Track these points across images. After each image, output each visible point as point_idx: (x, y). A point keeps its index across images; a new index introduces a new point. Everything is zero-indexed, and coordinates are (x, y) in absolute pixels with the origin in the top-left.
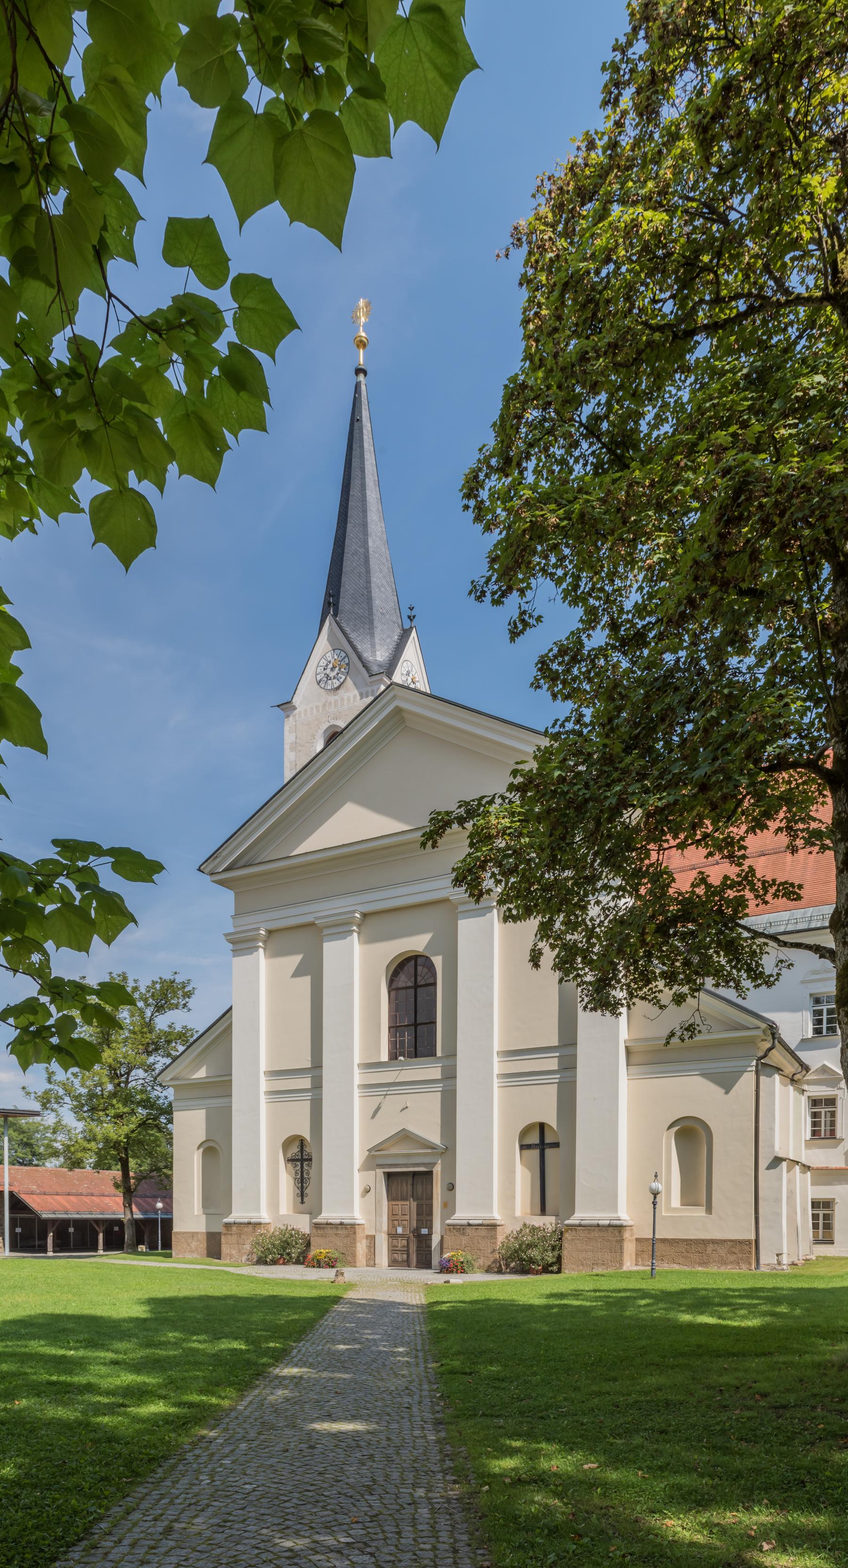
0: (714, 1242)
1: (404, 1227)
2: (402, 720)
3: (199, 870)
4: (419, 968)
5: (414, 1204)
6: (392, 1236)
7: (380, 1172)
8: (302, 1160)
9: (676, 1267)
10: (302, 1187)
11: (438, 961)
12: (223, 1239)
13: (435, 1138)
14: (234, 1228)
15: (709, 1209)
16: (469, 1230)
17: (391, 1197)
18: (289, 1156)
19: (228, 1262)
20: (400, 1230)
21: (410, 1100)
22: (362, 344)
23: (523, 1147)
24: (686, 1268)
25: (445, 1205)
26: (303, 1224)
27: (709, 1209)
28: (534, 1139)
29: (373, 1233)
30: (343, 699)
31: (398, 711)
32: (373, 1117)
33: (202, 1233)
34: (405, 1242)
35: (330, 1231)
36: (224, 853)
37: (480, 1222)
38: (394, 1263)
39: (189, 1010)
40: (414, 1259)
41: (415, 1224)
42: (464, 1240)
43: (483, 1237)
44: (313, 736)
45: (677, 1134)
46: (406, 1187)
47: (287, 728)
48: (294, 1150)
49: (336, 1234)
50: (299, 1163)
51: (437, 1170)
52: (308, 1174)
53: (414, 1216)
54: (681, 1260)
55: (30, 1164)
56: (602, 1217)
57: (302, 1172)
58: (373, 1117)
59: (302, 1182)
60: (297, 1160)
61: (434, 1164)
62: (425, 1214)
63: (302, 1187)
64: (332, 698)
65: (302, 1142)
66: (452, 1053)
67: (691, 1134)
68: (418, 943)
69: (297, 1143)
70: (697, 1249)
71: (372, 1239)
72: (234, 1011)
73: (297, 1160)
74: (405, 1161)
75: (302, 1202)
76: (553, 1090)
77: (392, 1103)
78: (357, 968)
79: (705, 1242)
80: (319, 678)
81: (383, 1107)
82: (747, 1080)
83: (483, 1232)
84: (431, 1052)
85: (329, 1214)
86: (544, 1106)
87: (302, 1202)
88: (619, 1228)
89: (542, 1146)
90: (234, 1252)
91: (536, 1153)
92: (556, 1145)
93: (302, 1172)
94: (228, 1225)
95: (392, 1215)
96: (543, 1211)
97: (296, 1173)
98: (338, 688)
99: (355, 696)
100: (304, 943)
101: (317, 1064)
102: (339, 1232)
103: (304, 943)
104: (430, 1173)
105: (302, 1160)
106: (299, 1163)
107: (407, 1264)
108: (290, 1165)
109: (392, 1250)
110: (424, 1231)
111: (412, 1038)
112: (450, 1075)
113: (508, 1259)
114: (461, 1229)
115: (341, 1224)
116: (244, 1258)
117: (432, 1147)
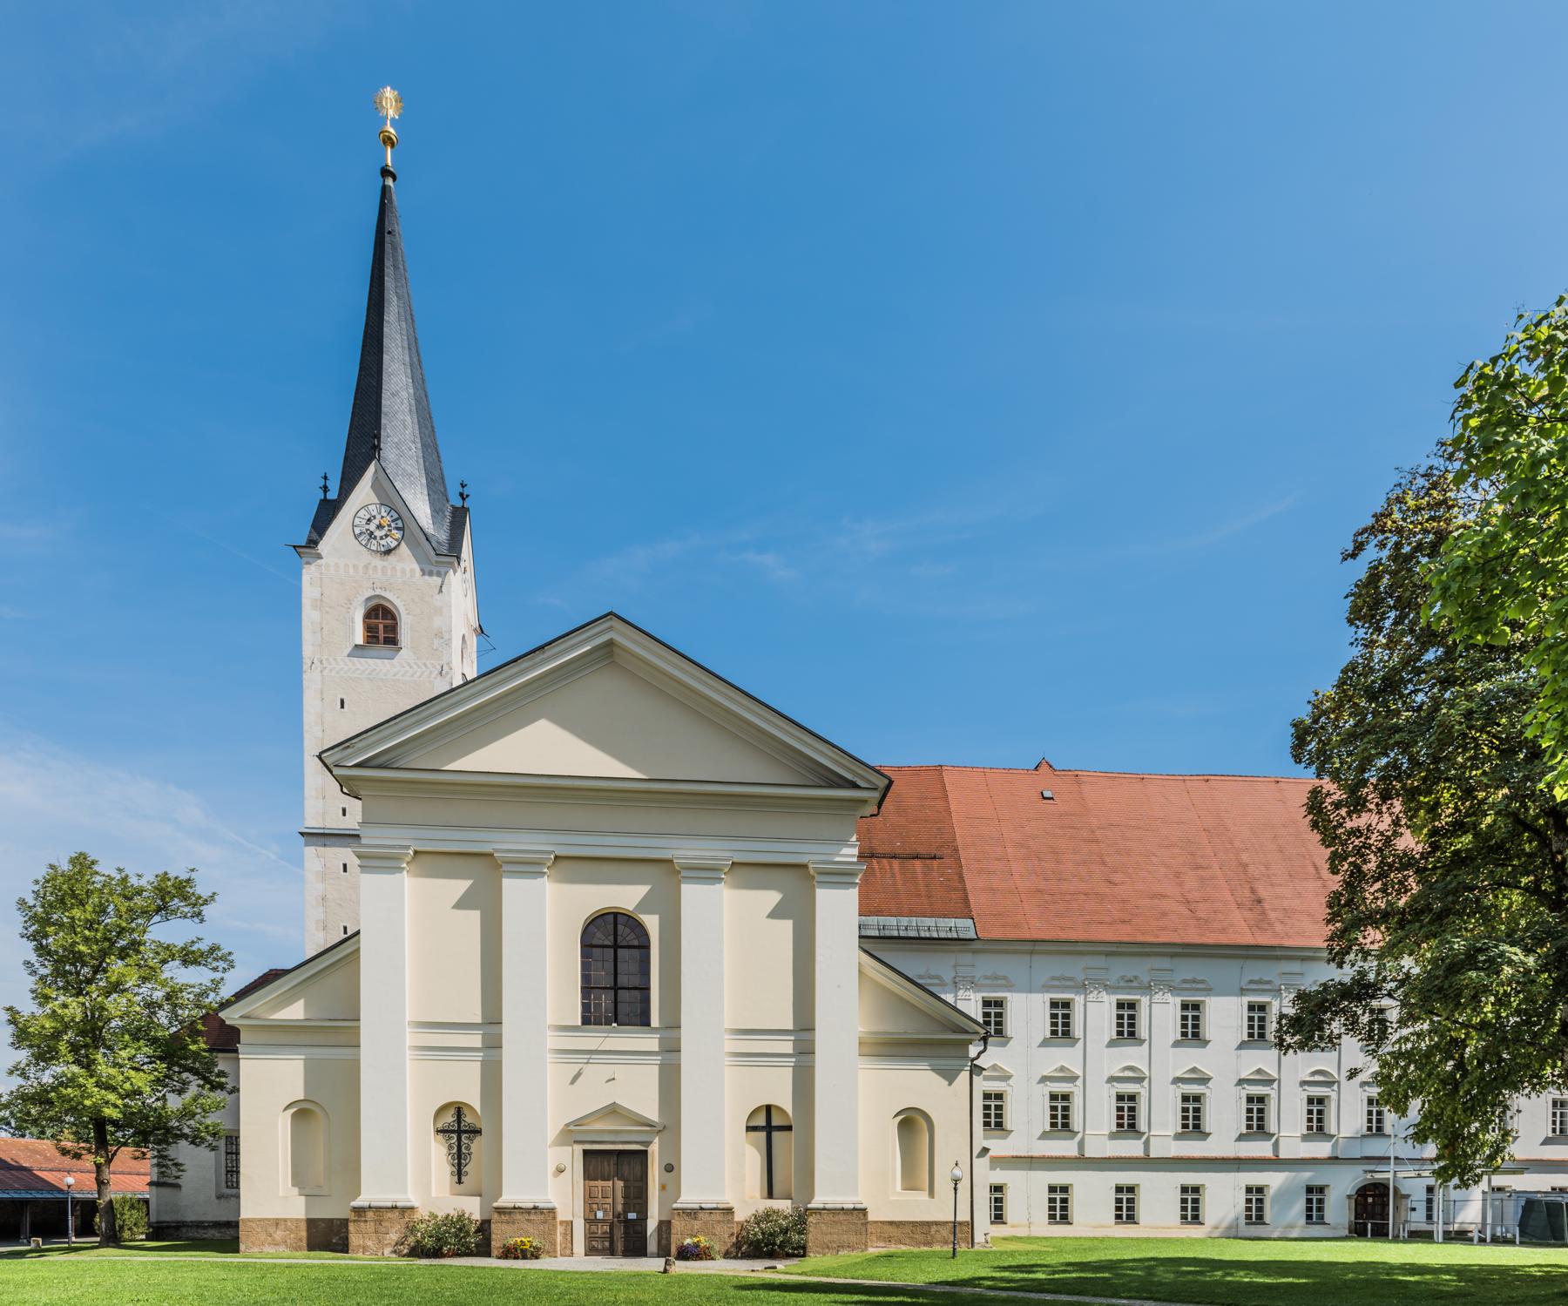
0: (936, 1223)
1: (605, 1211)
2: (611, 654)
3: (319, 757)
4: (620, 928)
5: (620, 1184)
6: (590, 1221)
7: (579, 1149)
9: (904, 1248)
10: (459, 1164)
11: (651, 923)
12: (351, 1227)
14: (370, 1215)
15: (931, 1193)
16: (701, 1215)
17: (588, 1176)
18: (440, 1126)
19: (360, 1255)
20: (600, 1215)
21: (619, 1071)
22: (388, 141)
23: (750, 1129)
24: (916, 1250)
26: (473, 1209)
27: (931, 1193)
28: (761, 1121)
30: (394, 568)
31: (610, 644)
32: (573, 1082)
34: (607, 1228)
35: (518, 1217)
36: (360, 745)
38: (591, 1251)
39: (202, 921)
40: (619, 1246)
41: (620, 1208)
42: (697, 1225)
44: (350, 601)
45: (293, 1115)
46: (608, 1166)
47: (306, 578)
48: (449, 1119)
51: (654, 1149)
52: (468, 1148)
53: (620, 1200)
54: (355, 1275)
56: (847, 1201)
57: (459, 1147)
58: (573, 1082)
59: (459, 1158)
61: (648, 1143)
62: (637, 1196)
64: (378, 562)
65: (459, 1110)
66: (673, 1025)
67: (911, 1123)
68: (626, 896)
69: (452, 1111)
70: (921, 1230)
72: (365, 941)
74: (612, 1138)
75: (460, 1182)
76: (787, 1074)
77: (596, 1073)
78: (548, 919)
79: (929, 1224)
80: (357, 531)
81: (585, 1073)
82: (964, 1076)
83: (717, 1216)
84: (642, 1019)
86: (778, 1089)
87: (460, 1182)
88: (552, 1211)
89: (769, 1129)
90: (370, 1243)
92: (789, 1128)
93: (459, 1147)
94: (359, 1211)
95: (589, 1197)
96: (770, 1195)
97: (450, 1147)
98: (388, 552)
99: (412, 571)
100: (484, 875)
101: (492, 1020)
102: (532, 1217)
103: (484, 875)
104: (643, 1154)
105: (459, 1132)
107: (611, 1252)
108: (440, 1136)
109: (590, 1237)
110: (632, 1216)
111: (610, 1003)
112: (671, 1049)
113: (738, 1245)
114: (692, 1213)
115: (535, 1208)
116: (387, 1251)
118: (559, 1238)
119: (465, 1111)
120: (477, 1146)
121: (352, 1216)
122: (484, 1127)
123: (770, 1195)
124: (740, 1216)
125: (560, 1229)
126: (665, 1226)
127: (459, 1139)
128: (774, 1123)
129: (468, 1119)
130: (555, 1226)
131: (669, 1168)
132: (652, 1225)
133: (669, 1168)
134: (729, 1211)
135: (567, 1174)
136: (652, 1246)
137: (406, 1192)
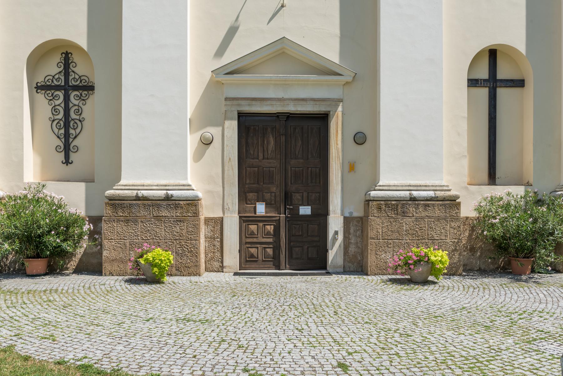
6: (246, 220)
8: (67, 88)
10: (67, 135)
13: (330, 51)
18: (40, 79)
23: (473, 83)
25: (351, 167)
29: (219, 214)
32: (268, 23)
33: (525, 188)
37: (431, 194)
38: (248, 262)
43: (438, 219)
48: (52, 69)
49: (158, 218)
50: (60, 94)
52: (79, 112)
55: (425, 282)
58: (268, 23)
59: (67, 126)
60: (58, 88)
63: (67, 135)
65: (66, 54)
69: (57, 58)
71: (218, 224)
73: (58, 88)
85: (138, 176)
87: (67, 161)
88: (193, 203)
89: (493, 83)
91: (483, 93)
92: (520, 83)
96: (492, 178)
97: (55, 110)
105: (67, 88)
106: (61, 94)
108: (41, 97)
114: (398, 207)
115: (168, 198)
117: (325, 70)
118: (203, 244)
119: (76, 58)
120: (92, 109)
121: (107, 212)
122: (98, 80)
123: (492, 178)
124: (468, 210)
125: (203, 231)
126: (356, 225)
127: (67, 99)
128: (500, 76)
129: (80, 69)
130: (197, 227)
131: (360, 139)
132: (335, 224)
133: (360, 139)
134: (452, 203)
135: (215, 150)
136: (334, 254)
137: (186, 179)
